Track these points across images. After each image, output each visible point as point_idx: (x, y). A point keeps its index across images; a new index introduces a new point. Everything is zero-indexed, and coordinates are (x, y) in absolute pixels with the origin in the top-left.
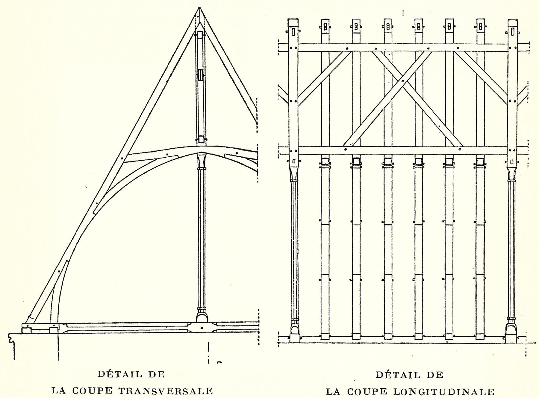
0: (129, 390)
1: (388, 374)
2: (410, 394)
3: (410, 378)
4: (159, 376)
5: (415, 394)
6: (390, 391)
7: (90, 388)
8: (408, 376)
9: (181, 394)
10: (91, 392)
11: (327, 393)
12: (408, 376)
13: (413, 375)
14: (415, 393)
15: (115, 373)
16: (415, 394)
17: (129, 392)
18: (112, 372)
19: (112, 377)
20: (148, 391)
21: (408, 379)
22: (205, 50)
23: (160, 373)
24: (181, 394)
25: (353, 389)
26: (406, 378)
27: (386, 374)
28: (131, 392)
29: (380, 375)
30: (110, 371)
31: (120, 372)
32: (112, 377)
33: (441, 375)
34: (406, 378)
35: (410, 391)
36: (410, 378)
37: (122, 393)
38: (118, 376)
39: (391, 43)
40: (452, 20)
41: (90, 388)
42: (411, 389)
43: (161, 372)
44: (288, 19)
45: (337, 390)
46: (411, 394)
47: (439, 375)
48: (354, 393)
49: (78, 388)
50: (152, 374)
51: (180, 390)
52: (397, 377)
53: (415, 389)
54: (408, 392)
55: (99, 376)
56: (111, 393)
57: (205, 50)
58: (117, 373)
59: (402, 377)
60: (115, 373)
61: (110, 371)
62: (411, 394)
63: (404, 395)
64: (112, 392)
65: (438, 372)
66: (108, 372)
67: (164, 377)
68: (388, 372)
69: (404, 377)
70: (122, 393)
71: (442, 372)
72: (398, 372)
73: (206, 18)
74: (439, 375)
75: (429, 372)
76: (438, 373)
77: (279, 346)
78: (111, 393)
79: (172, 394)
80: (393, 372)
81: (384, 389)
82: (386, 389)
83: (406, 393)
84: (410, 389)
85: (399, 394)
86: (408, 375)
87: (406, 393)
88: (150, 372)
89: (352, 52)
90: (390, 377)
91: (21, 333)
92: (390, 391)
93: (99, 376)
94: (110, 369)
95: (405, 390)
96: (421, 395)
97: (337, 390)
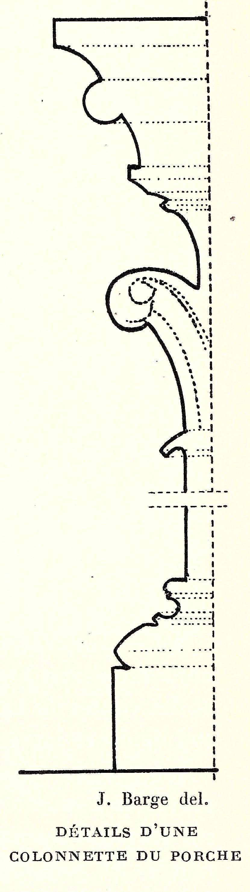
0: (199, 854)
1: (73, 831)
2: (58, 860)
3: (107, 836)
5: (78, 860)
6: (132, 856)
7: (152, 852)
8: (103, 833)
9: (203, 860)
10: (154, 859)
12: (103, 833)
13: (111, 833)
16: (78, 860)
17: (199, 858)
18: (77, 829)
19: (196, 835)
20: (64, 856)
21: (103, 839)
24: (203, 860)
25: (17, 853)
28: (202, 857)
29: (62, 832)
30: (75, 827)
31: (89, 828)
34: (100, 836)
35: (57, 854)
36: (107, 836)
37: (110, 860)
38: (99, 860)
39: (207, 124)
40: (57, 23)
41: (152, 852)
42: (72, 852)
44: (55, 20)
47: (192, 831)
48: (20, 859)
49: (17, 853)
50: (143, 856)
51: (202, 854)
52: (87, 835)
53: (78, 852)
54: (55, 857)
55: (59, 835)
56: (126, 859)
60: (106, 854)
63: (186, 861)
64: (126, 857)
66: (71, 829)
70: (110, 860)
74: (192, 831)
78: (126, 859)
79: (239, 860)
80: (82, 828)
81: (122, 852)
83: (51, 859)
85: (41, 860)
88: (143, 828)
91: (111, 768)
92: (132, 856)
93: (59, 835)
94: (74, 825)
95: (188, 853)
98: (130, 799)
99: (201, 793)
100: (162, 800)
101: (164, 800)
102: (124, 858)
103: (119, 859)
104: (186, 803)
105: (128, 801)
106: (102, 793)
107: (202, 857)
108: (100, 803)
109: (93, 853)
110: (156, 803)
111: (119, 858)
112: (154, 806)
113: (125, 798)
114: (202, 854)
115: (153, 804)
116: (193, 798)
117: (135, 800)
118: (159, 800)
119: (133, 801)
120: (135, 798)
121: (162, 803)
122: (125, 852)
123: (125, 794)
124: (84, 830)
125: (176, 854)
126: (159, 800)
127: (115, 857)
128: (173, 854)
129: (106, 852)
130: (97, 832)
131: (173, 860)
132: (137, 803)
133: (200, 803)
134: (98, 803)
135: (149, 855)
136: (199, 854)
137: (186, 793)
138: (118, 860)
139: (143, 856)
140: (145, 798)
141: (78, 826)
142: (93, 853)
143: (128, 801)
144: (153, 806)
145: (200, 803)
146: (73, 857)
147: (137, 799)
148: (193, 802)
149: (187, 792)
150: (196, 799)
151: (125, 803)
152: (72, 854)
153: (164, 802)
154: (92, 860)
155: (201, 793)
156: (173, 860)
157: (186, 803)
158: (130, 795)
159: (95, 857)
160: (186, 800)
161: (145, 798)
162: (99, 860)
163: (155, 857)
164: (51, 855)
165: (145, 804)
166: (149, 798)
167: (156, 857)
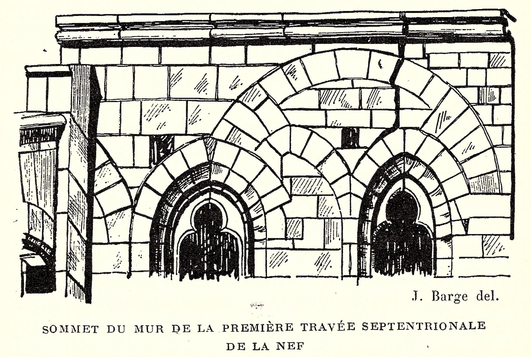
0: (313, 325)
1: (341, 325)
3: (263, 331)
4: (185, 331)
6: (249, 346)
7: (119, 326)
11: (238, 349)
14: (283, 348)
15: (92, 327)
18: (272, 325)
19: (190, 331)
22: (489, 137)
23: (479, 324)
26: (465, 329)
27: (339, 325)
28: (315, 328)
32: (190, 331)
33: (271, 327)
34: (465, 329)
38: (420, 329)
41: (119, 326)
42: (279, 343)
43: (375, 323)
45: (265, 345)
46: (279, 349)
50: (111, 329)
55: (109, 332)
56: (244, 349)
57: (489, 137)
58: (93, 327)
59: (462, 328)
60: (92, 327)
61: (342, 323)
62: (279, 349)
65: (184, 326)
67: (292, 330)
68: (342, 323)
69: (464, 328)
71: (189, 326)
72: (98, 326)
73: (201, 80)
75: (109, 326)
76: (373, 325)
77: (497, 299)
78: (244, 349)
80: (92, 326)
82: (303, 343)
84: (278, 343)
86: (467, 326)
87: (234, 348)
88: (174, 326)
89: (283, 106)
90: (343, 329)
92: (249, 346)
94: (341, 321)
96: (54, 332)
97: (265, 345)
98: (438, 296)
99: (493, 291)
100: (463, 297)
101: (465, 296)
102: (483, 327)
103: (399, 329)
104: (482, 299)
105: (436, 298)
106: (416, 292)
107: (315, 328)
108: (414, 299)
109: (90, 327)
110: (458, 299)
111: (373, 328)
112: (457, 302)
113: (434, 296)
114: (431, 324)
115: (456, 300)
116: (487, 296)
117: (442, 297)
118: (461, 297)
119: (440, 297)
120: (442, 296)
121: (463, 299)
122: (244, 344)
123: (434, 292)
124: (390, 324)
125: (226, 327)
126: (461, 297)
127: (395, 327)
128: (224, 327)
129: (92, 326)
130: (463, 326)
131: (224, 331)
132: (443, 299)
133: (493, 299)
134: (413, 299)
135: (117, 328)
136: (313, 325)
137: (481, 291)
138: (390, 330)
139: (111, 329)
140: (449, 295)
141: (345, 322)
142: (90, 327)
143: (436, 298)
144: (456, 302)
145: (493, 299)
146: (453, 327)
147: (443, 296)
148: (487, 298)
149: (493, 291)
150: (489, 296)
151: (434, 300)
152: (451, 324)
153: (465, 299)
154: (89, 332)
155: (493, 291)
156: (224, 331)
157: (482, 299)
158: (438, 293)
159: (92, 330)
160: (482, 296)
161: (449, 295)
162: (95, 332)
163: (121, 330)
164: (114, 328)
165: (449, 299)
166: (452, 295)
167: (122, 329)
